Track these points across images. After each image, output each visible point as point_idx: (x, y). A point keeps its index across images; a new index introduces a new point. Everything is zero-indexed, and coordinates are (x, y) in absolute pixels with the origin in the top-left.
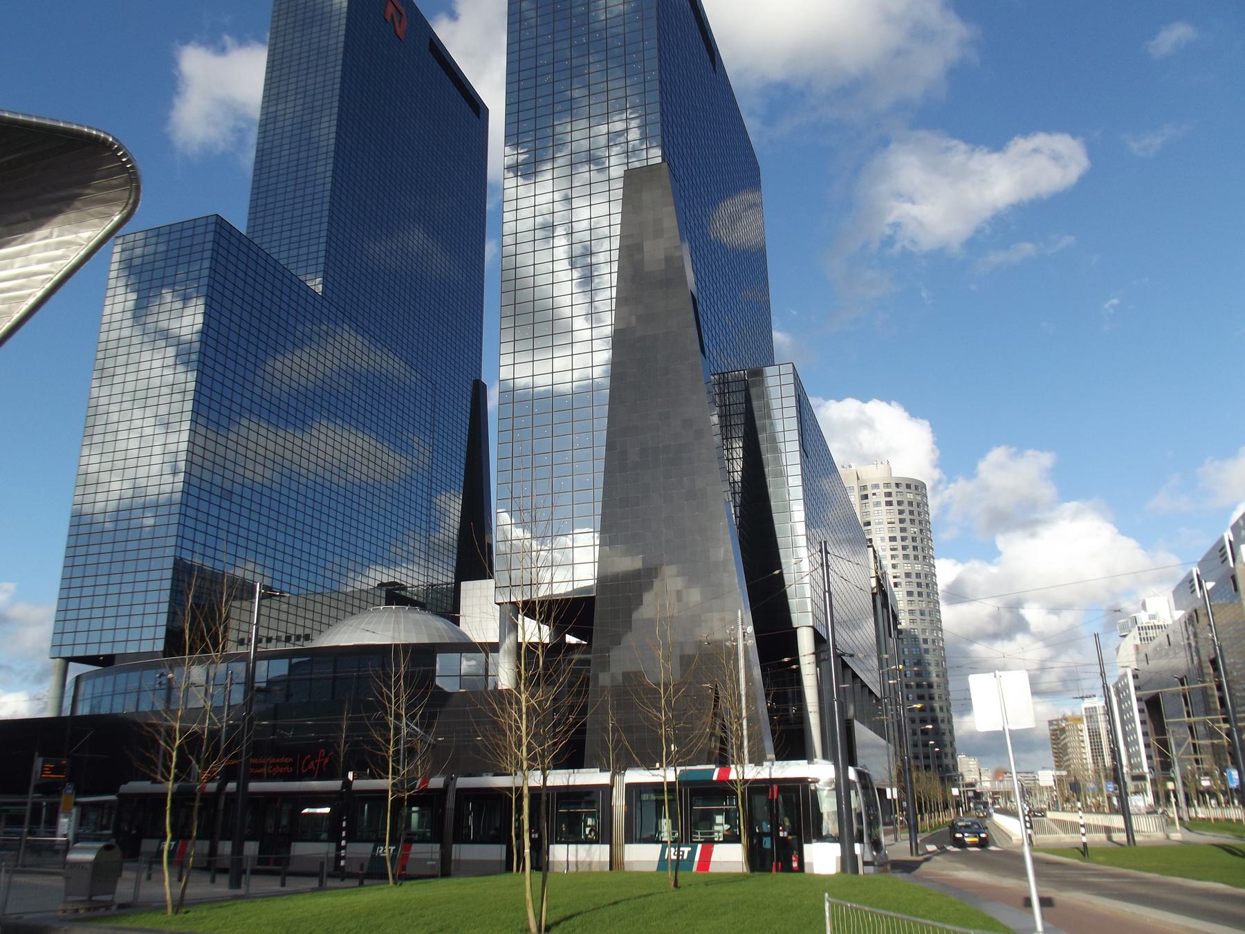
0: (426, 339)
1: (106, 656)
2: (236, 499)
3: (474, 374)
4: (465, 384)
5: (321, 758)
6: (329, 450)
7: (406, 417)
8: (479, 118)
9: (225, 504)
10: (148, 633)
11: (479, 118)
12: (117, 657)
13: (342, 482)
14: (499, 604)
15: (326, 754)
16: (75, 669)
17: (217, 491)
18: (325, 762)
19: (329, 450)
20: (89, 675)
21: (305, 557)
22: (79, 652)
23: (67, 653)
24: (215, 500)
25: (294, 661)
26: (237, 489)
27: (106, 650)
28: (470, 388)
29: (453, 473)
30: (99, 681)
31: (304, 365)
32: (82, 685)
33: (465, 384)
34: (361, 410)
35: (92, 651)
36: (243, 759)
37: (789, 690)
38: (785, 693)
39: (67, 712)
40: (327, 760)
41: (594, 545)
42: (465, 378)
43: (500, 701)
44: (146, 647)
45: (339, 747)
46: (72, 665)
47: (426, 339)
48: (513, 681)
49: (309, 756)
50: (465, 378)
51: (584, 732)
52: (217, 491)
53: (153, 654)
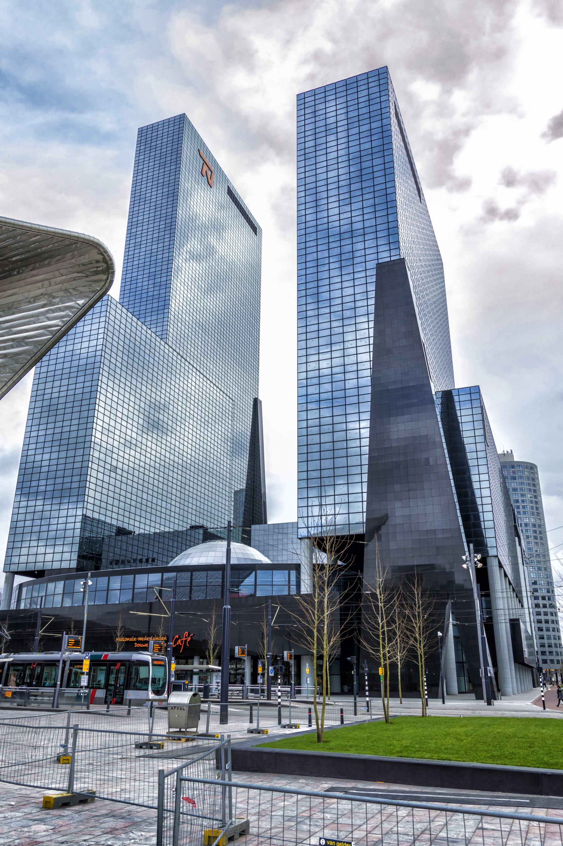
0: (215, 362)
1: (39, 572)
2: (119, 472)
3: (254, 394)
4: (249, 401)
5: (186, 637)
6: (181, 446)
7: (223, 426)
8: (256, 234)
9: (113, 475)
10: (66, 556)
11: (256, 234)
12: (46, 572)
13: (180, 461)
14: (300, 539)
15: (189, 636)
16: (19, 580)
17: (108, 467)
18: (188, 640)
19: (181, 446)
20: (27, 584)
21: (111, 494)
22: (22, 568)
23: (14, 568)
24: (107, 472)
25: (166, 575)
26: (120, 465)
27: (39, 567)
28: (252, 403)
29: (213, 432)
30: (37, 586)
31: (158, 393)
32: (24, 589)
33: (249, 401)
34: (191, 417)
35: (31, 567)
36: (326, 614)
37: (83, 639)
38: (264, 693)
39: (13, 607)
40: (189, 639)
41: (370, 352)
42: (249, 397)
43: (311, 602)
44: (65, 565)
45: (210, 630)
46: (17, 577)
47: (215, 362)
48: (312, 590)
49: (177, 636)
50: (249, 397)
51: (341, 620)
52: (108, 467)
53: (69, 570)
